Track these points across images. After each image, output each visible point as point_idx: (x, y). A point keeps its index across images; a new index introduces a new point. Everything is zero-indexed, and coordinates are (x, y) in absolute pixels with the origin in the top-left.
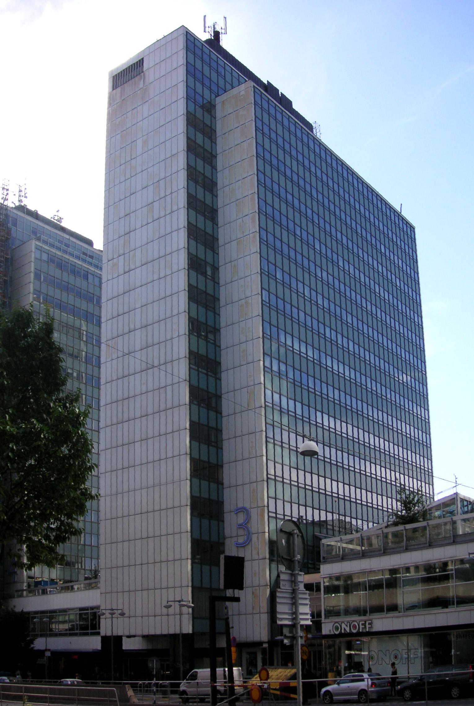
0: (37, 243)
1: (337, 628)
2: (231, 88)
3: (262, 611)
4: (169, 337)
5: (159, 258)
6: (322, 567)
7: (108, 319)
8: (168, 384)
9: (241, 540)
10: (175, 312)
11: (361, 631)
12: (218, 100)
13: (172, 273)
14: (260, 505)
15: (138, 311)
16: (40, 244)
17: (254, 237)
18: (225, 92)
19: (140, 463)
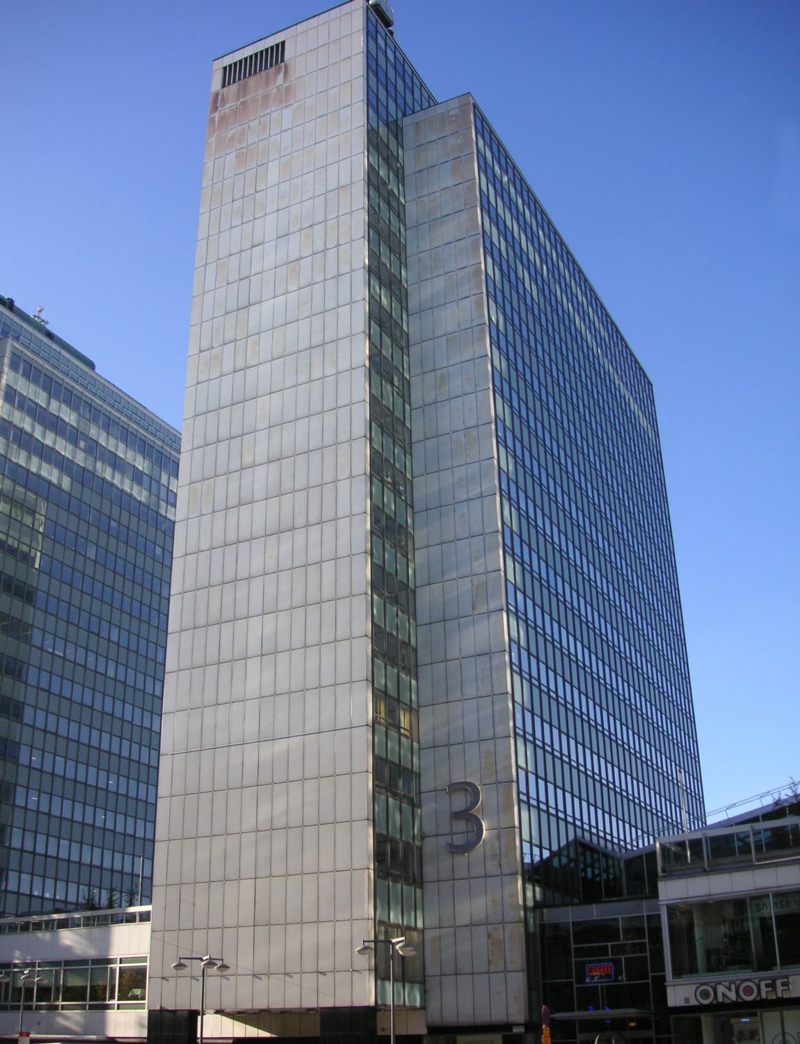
0: (15, 344)
1: (705, 994)
2: (420, 109)
3: (510, 967)
4: (329, 477)
5: (311, 348)
6: (662, 886)
7: (195, 446)
8: (325, 558)
9: (459, 840)
10: (343, 436)
11: (764, 996)
12: (407, 122)
13: (338, 373)
14: (501, 777)
15: (262, 435)
16: (21, 348)
17: (483, 332)
18: (414, 112)
19: (271, 692)
